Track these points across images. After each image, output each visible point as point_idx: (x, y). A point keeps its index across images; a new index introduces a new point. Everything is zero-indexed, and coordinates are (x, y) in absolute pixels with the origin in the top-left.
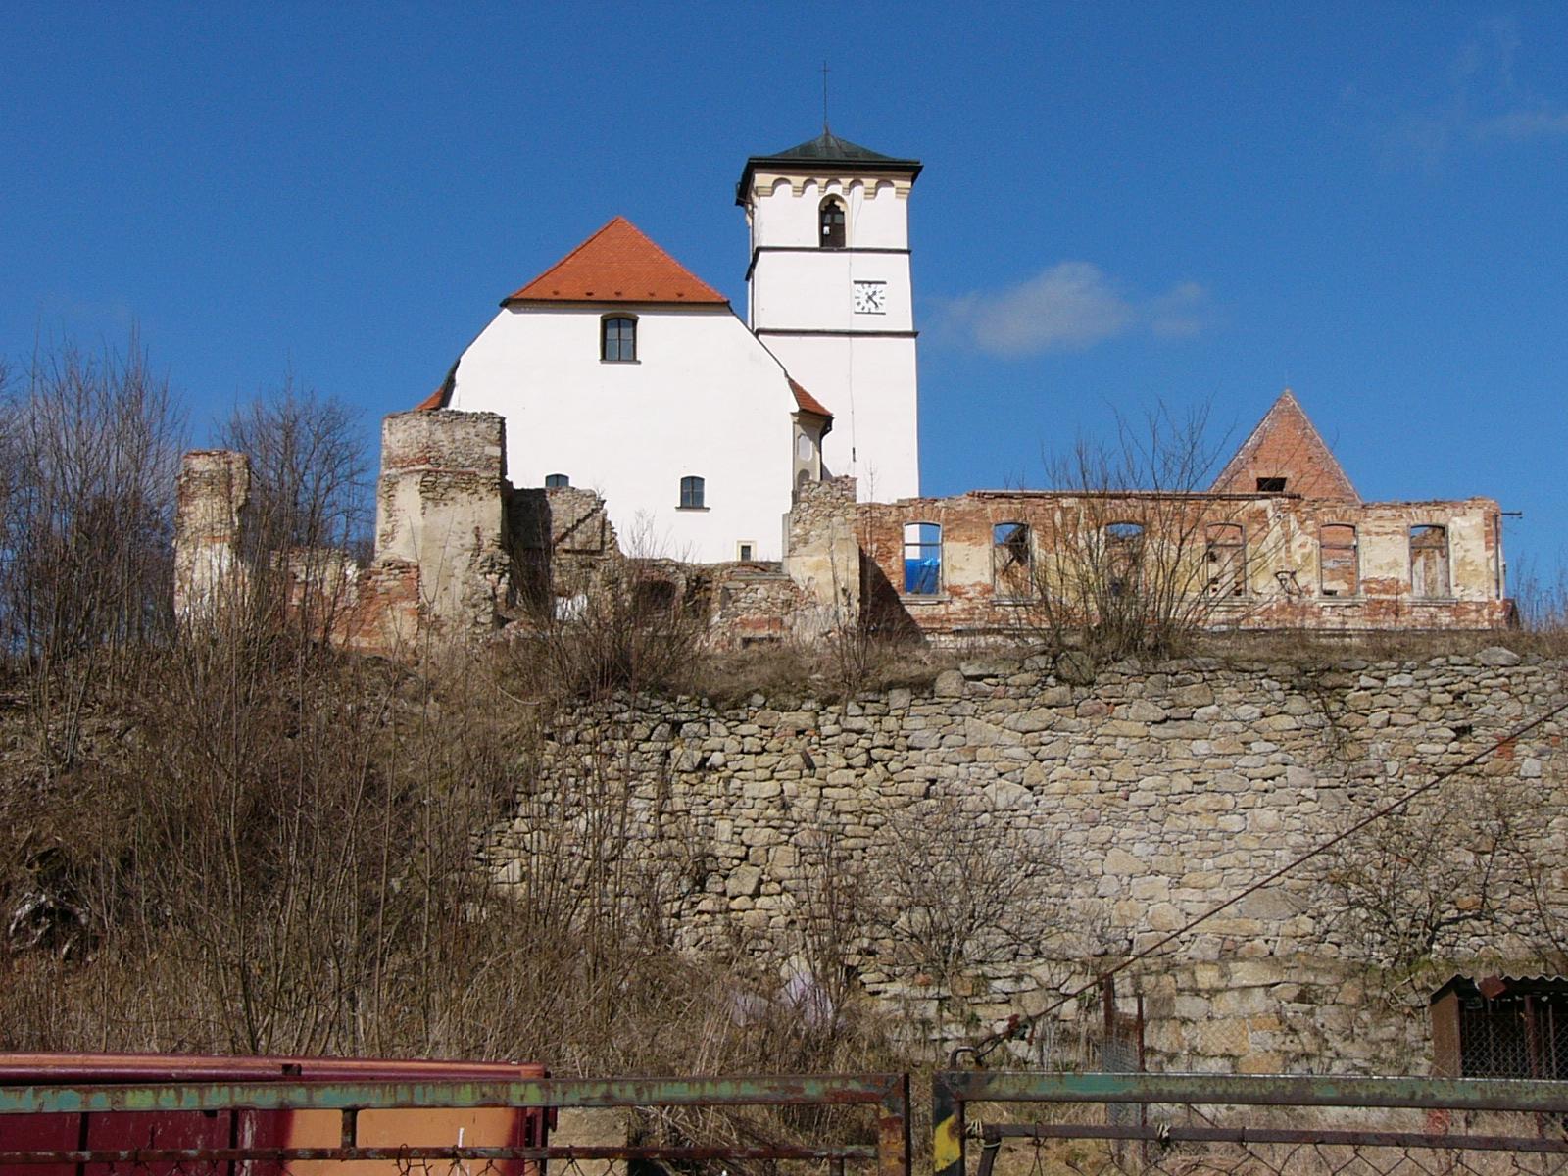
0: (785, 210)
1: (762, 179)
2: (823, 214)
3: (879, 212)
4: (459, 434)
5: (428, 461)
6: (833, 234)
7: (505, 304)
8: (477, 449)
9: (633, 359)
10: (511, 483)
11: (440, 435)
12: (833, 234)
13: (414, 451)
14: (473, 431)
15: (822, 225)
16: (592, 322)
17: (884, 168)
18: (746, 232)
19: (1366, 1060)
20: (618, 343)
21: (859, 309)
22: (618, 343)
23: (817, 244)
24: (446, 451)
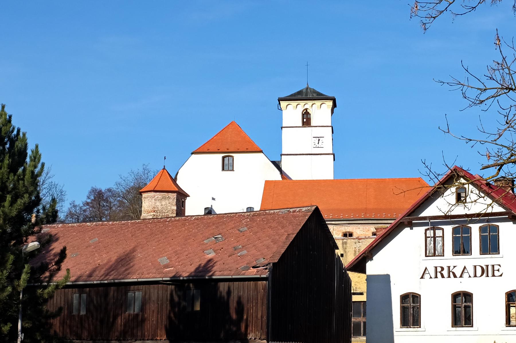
0: (292, 113)
1: (283, 104)
2: (303, 115)
3: (321, 112)
4: (164, 203)
5: (154, 211)
6: (306, 120)
7: (192, 154)
8: (169, 207)
9: (233, 170)
10: (250, 209)
11: (158, 204)
12: (306, 120)
13: (150, 209)
14: (168, 202)
15: (303, 119)
16: (219, 157)
17: (320, 97)
18: (280, 118)
19: (239, 298)
20: (227, 166)
21: (315, 146)
22: (227, 166)
23: (301, 125)
24: (160, 209)
